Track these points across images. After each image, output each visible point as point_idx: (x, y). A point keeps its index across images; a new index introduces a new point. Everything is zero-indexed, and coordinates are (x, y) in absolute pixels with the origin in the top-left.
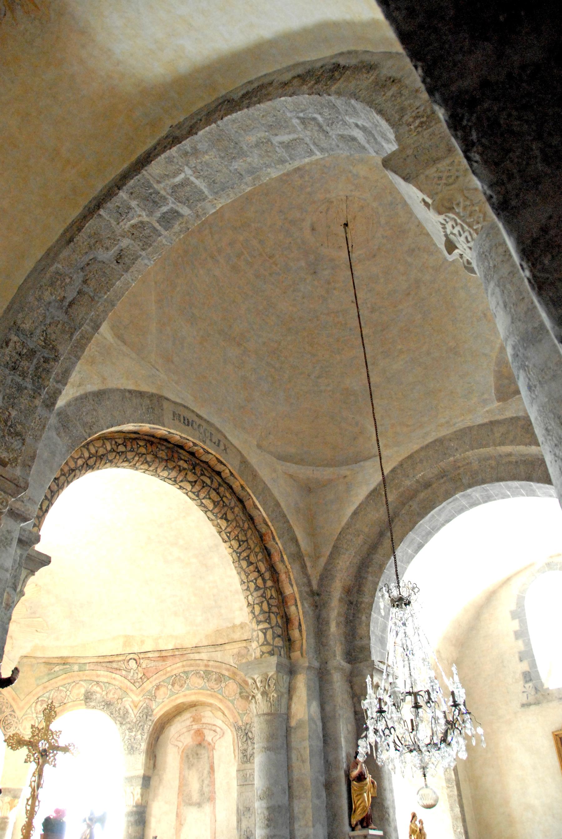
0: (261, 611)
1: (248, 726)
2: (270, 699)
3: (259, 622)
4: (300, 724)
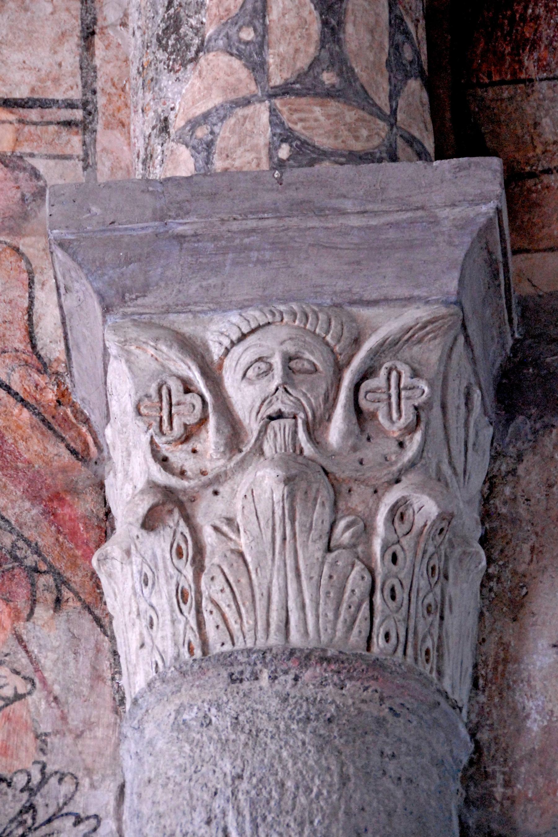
2: (367, 529)
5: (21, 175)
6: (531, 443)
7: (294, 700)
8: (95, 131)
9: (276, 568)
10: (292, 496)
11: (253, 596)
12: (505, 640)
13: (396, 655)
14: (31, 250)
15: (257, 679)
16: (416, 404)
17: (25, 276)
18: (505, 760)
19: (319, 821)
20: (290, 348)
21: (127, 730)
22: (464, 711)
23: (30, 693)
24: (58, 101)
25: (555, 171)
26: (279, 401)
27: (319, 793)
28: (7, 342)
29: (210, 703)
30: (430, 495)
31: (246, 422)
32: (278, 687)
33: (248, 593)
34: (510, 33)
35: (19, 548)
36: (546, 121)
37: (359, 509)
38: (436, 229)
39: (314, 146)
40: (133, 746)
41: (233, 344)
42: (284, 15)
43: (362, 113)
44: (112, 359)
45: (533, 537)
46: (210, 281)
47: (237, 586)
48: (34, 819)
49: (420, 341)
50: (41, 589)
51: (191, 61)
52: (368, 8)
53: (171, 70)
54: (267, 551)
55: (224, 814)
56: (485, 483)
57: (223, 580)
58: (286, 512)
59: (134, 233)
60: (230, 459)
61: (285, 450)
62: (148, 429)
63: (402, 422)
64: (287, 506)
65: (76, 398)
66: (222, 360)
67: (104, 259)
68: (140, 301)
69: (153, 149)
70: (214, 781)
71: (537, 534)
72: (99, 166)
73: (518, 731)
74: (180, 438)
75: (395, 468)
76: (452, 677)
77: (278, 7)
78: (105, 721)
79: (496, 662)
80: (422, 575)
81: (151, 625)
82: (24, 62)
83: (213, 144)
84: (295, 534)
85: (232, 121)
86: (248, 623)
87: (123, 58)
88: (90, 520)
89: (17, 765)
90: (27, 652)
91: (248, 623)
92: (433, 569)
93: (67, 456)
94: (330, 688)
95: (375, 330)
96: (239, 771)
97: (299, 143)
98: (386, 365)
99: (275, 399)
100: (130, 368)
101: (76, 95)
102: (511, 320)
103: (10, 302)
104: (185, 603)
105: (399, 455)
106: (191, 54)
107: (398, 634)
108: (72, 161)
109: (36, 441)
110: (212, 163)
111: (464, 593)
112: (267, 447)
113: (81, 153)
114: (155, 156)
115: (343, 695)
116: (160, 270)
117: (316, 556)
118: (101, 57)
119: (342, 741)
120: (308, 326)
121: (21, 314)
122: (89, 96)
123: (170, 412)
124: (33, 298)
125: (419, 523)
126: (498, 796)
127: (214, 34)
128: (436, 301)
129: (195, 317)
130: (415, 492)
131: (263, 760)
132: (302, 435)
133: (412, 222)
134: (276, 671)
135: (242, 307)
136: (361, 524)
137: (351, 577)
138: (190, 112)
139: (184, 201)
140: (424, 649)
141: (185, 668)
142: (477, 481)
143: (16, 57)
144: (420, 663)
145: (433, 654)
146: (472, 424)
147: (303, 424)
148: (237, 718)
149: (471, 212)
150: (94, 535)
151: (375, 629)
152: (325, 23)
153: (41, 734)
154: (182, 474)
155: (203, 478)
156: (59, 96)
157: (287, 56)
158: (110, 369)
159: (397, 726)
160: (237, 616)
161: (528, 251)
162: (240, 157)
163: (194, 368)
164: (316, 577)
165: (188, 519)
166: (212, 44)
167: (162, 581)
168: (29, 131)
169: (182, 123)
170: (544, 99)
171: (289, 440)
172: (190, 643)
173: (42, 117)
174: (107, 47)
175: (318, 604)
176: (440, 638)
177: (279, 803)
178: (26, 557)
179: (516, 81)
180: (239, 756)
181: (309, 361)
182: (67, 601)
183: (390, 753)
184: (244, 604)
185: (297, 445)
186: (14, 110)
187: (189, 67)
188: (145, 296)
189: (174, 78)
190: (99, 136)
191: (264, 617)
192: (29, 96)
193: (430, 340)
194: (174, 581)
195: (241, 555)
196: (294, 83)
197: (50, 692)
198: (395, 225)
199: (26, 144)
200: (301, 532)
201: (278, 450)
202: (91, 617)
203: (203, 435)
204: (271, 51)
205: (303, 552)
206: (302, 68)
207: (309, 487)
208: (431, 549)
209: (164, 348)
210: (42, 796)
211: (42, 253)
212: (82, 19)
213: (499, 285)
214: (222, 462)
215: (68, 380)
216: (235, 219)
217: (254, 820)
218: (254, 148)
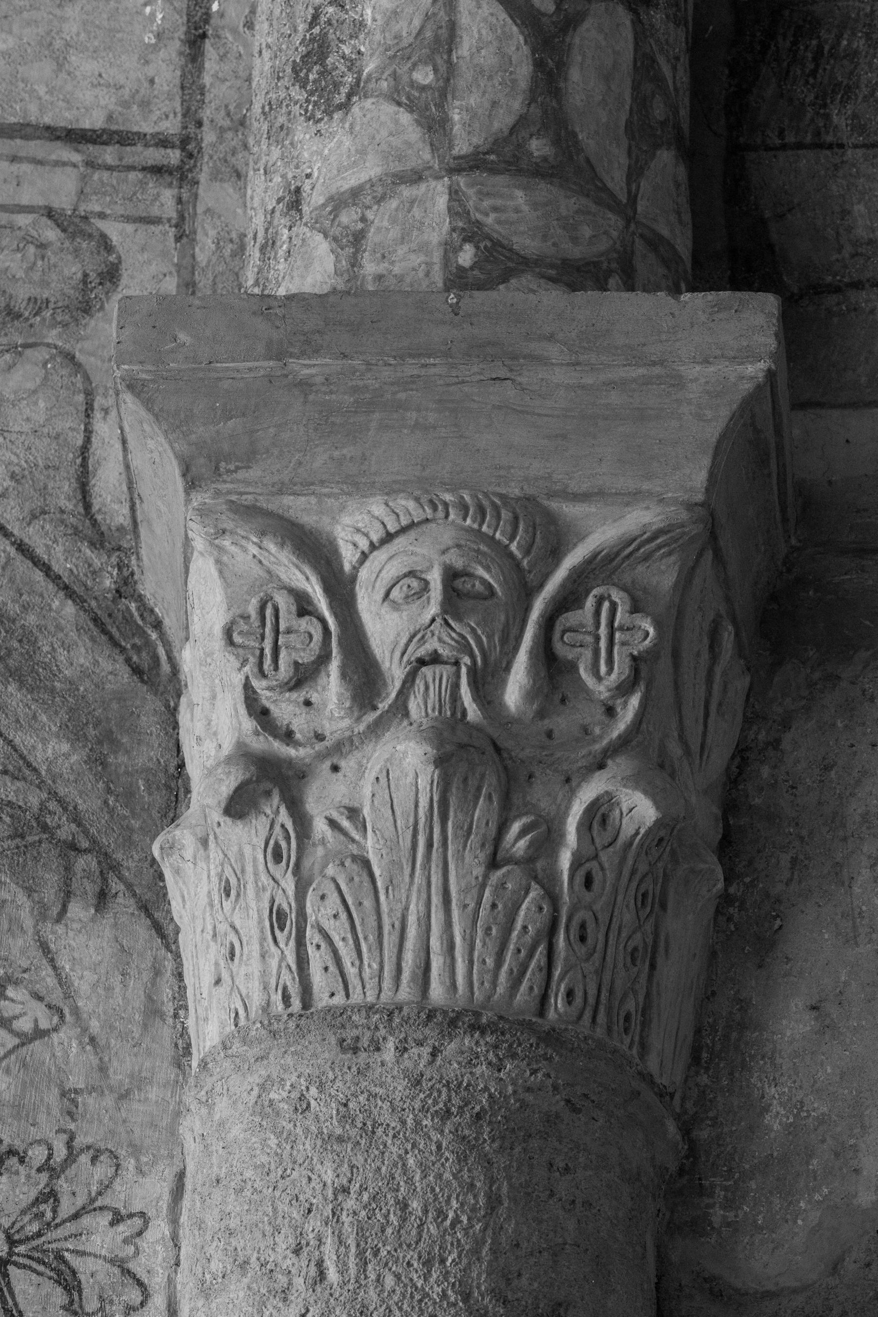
5: (84, 245)
6: (804, 702)
7: (430, 1084)
8: (197, 183)
9: (415, 888)
11: (380, 927)
13: (581, 1023)
15: (378, 1049)
16: (635, 653)
17: (80, 398)
18: (730, 1170)
19: (453, 1261)
21: (189, 1098)
22: (677, 1097)
23: (55, 1030)
24: (145, 135)
25: (867, 286)
26: (435, 638)
27: (456, 1221)
28: (49, 498)
29: (310, 1079)
30: (645, 793)
31: (385, 665)
32: (407, 1063)
33: (372, 922)
35: (50, 813)
36: (859, 209)
41: (373, 547)
43: (584, 201)
44: (195, 554)
46: (345, 451)
47: (357, 910)
48: (55, 1211)
49: (647, 558)
50: (79, 876)
51: (340, 107)
52: (604, 43)
54: (404, 861)
55: (320, 1241)
56: (733, 758)
57: (338, 901)
58: (435, 805)
60: (358, 719)
61: (440, 712)
64: (436, 798)
66: (356, 569)
67: (191, 410)
68: (241, 475)
69: (276, 233)
70: (309, 1192)
72: (199, 236)
74: (287, 683)
75: (597, 747)
77: (472, 37)
80: (627, 906)
82: (100, 75)
83: (364, 237)
85: (394, 204)
87: (243, 74)
88: (155, 775)
90: (55, 968)
91: (370, 966)
92: (645, 896)
94: (482, 1069)
95: (582, 538)
97: (489, 244)
98: (595, 592)
99: (429, 634)
100: (221, 572)
101: (171, 126)
102: (785, 520)
103: (57, 437)
104: (282, 929)
105: (606, 728)
106: (340, 98)
107: (585, 993)
108: (160, 227)
109: (83, 650)
110: (361, 266)
111: (686, 927)
112: (414, 705)
113: (174, 215)
114: (278, 244)
115: (501, 1079)
116: (272, 430)
117: (475, 873)
118: (212, 72)
119: (496, 1145)
120: (484, 528)
121: (71, 455)
122: (192, 129)
124: (91, 432)
126: (716, 1220)
128: (675, 502)
129: (320, 502)
130: (625, 786)
131: (379, 1169)
132: (465, 691)
134: (406, 1039)
135: (390, 490)
136: (544, 828)
137: (524, 907)
138: (332, 192)
140: (623, 1014)
141: (275, 1026)
142: (719, 758)
144: (615, 1035)
146: (718, 678)
147: (468, 673)
148: (346, 1105)
149: (731, 371)
150: (159, 799)
151: (554, 985)
152: (539, 65)
153: (70, 1090)
154: (288, 736)
155: (319, 746)
156: (147, 128)
157: (480, 111)
158: (193, 567)
160: (354, 955)
161: (820, 405)
162: (400, 261)
163: (313, 579)
164: (472, 905)
166: (372, 85)
167: (250, 888)
168: (101, 180)
169: (321, 200)
171: (446, 696)
172: (285, 989)
173: (121, 159)
174: (222, 58)
176: (648, 995)
177: (399, 1231)
178: (59, 827)
180: (346, 1160)
181: (483, 581)
182: (116, 895)
183: (562, 1165)
184: (365, 938)
185: (459, 704)
186: (81, 147)
188: (249, 467)
189: (314, 130)
191: (394, 959)
194: (267, 895)
195: (366, 864)
196: (487, 153)
197: (85, 1030)
199: (94, 197)
200: (455, 835)
201: (430, 711)
202: (149, 922)
203: (322, 680)
204: (457, 103)
205: (457, 867)
208: (643, 868)
209: (272, 548)
210: (67, 1180)
212: (188, 15)
214: (346, 723)
217: (361, 1254)
218: (423, 248)
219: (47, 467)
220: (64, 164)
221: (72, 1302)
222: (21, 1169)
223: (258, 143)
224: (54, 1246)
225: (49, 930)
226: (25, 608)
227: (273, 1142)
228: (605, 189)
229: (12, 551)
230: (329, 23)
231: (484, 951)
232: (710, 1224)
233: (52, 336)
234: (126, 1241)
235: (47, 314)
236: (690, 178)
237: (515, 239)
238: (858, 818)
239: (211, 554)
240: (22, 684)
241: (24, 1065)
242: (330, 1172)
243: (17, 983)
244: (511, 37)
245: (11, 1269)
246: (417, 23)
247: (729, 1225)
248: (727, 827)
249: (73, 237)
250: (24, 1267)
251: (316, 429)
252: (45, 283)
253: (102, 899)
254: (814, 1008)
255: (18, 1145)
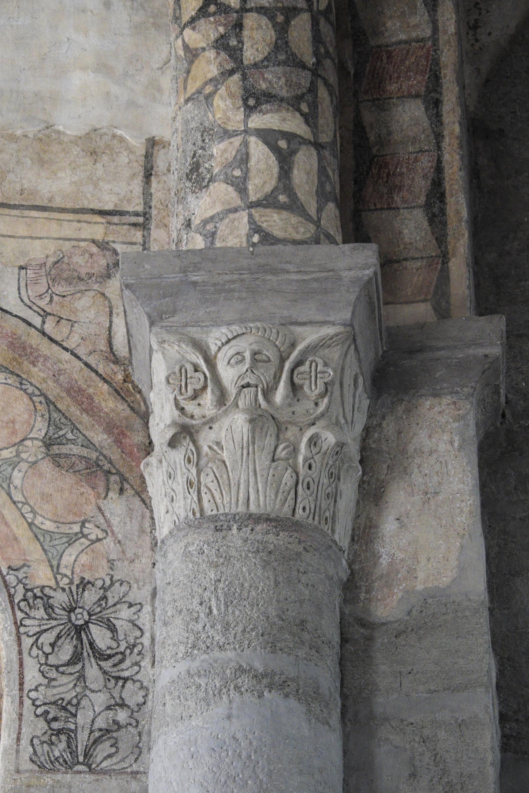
0: (277, 48)
1: (90, 597)
2: (295, 451)
3: (254, 99)
4: (430, 615)
5: (107, 253)
10: (253, 433)
11: (230, 485)
12: (371, 516)
14: (111, 295)
15: (230, 529)
20: (255, 347)
22: (346, 553)
23: (105, 538)
29: (204, 542)
30: (331, 432)
32: (242, 534)
33: (227, 482)
34: (387, 182)
36: (406, 231)
37: (291, 439)
38: (340, 283)
39: (273, 236)
40: (161, 565)
41: (223, 345)
42: (258, 162)
44: (154, 352)
45: (389, 461)
48: (106, 603)
49: (329, 346)
53: (193, 192)
55: (210, 600)
57: (213, 476)
59: (169, 280)
60: (219, 409)
62: (174, 391)
63: (317, 392)
64: (250, 436)
65: (135, 378)
66: (216, 354)
68: (171, 319)
70: (205, 582)
71: (391, 459)
73: (375, 564)
75: (312, 417)
76: (340, 534)
78: (146, 554)
79: (365, 528)
81: (173, 500)
84: (254, 451)
85: (227, 220)
86: (226, 499)
89: (97, 576)
90: (104, 516)
91: (226, 499)
92: (332, 474)
93: (128, 410)
95: (304, 339)
96: (219, 578)
100: (164, 357)
101: (140, 209)
103: (99, 324)
104: (192, 488)
105: (315, 410)
106: (204, 184)
111: (349, 490)
112: (240, 403)
113: (142, 241)
122: (147, 210)
123: (186, 382)
125: (324, 448)
126: (362, 598)
127: (218, 172)
132: (260, 397)
133: (326, 279)
135: (229, 324)
136: (292, 447)
139: (197, 263)
142: (359, 428)
143: (107, 187)
145: (330, 520)
151: (298, 505)
152: (281, 168)
154: (192, 417)
155: (204, 420)
156: (130, 209)
158: (153, 359)
159: (307, 557)
160: (220, 496)
163: (200, 358)
164: (266, 475)
165: (194, 442)
166: (217, 177)
169: (199, 222)
170: (405, 219)
172: (193, 510)
174: (159, 182)
175: (266, 490)
176: (334, 512)
179: (390, 209)
183: (303, 571)
187: (204, 190)
188: (174, 316)
190: (152, 232)
192: (114, 208)
193: (335, 346)
194: (185, 476)
195: (224, 462)
197: (116, 538)
198: (316, 280)
200: (258, 450)
203: (204, 396)
204: (250, 182)
206: (267, 192)
207: (263, 426)
208: (331, 463)
209: (184, 346)
211: (118, 297)
213: (375, 318)
214: (214, 411)
215: (130, 368)
216: (226, 274)
219: (96, 335)
220: (98, 223)
221: (114, 636)
222: (93, 588)
223: (173, 206)
224: (106, 616)
225: (100, 502)
226: (89, 386)
227: (190, 566)
228: (308, 215)
229: (83, 366)
230: (200, 156)
231: (271, 493)
232: (360, 599)
233: (96, 287)
234: (134, 614)
235: (94, 279)
236: (341, 214)
237: (274, 232)
238: (412, 451)
239: (160, 350)
240: (88, 414)
241: (93, 551)
242: (213, 575)
243: (89, 522)
244: (270, 157)
245: (90, 625)
246: (234, 153)
247: (367, 599)
248: (362, 456)
249: (103, 250)
250: (95, 624)
251: (200, 301)
252: (92, 268)
253: (121, 491)
254: (398, 519)
255: (92, 580)
